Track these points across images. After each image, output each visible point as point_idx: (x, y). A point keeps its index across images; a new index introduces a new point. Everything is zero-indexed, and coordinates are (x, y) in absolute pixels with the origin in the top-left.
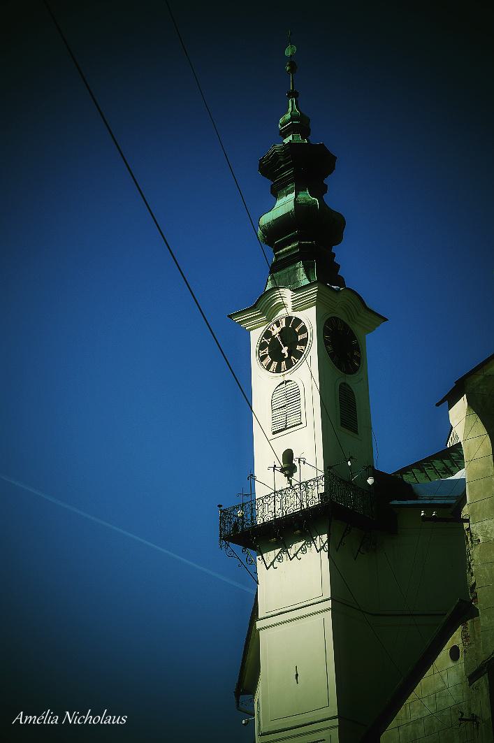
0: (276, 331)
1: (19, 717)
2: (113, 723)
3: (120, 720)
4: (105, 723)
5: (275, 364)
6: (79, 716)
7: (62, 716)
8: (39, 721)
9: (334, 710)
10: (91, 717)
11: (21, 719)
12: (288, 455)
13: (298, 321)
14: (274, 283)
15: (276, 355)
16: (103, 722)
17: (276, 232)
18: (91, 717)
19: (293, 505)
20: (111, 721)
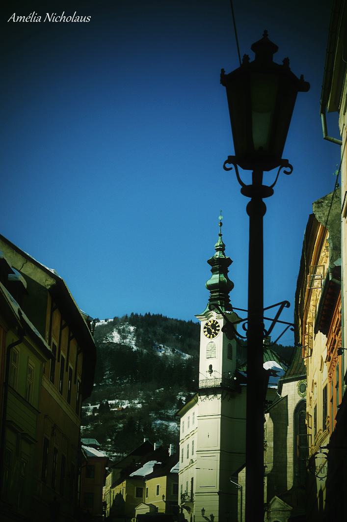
0: (210, 324)
1: (13, 17)
2: (81, 21)
3: (86, 19)
4: (75, 21)
5: (209, 335)
6: (56, 16)
7: (44, 16)
8: (27, 20)
9: (217, 490)
10: (65, 17)
11: (14, 18)
12: (211, 367)
13: (217, 323)
14: (209, 308)
15: (209, 332)
16: (73, 20)
17: (210, 287)
18: (65, 17)
19: (211, 384)
20: (79, 20)
